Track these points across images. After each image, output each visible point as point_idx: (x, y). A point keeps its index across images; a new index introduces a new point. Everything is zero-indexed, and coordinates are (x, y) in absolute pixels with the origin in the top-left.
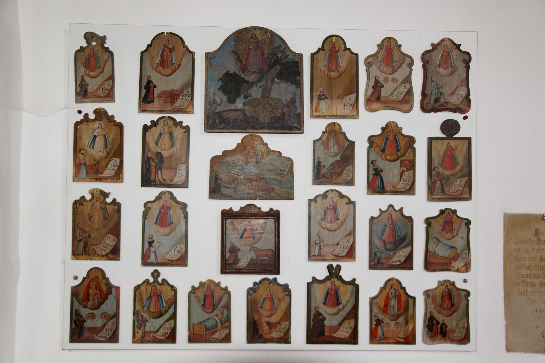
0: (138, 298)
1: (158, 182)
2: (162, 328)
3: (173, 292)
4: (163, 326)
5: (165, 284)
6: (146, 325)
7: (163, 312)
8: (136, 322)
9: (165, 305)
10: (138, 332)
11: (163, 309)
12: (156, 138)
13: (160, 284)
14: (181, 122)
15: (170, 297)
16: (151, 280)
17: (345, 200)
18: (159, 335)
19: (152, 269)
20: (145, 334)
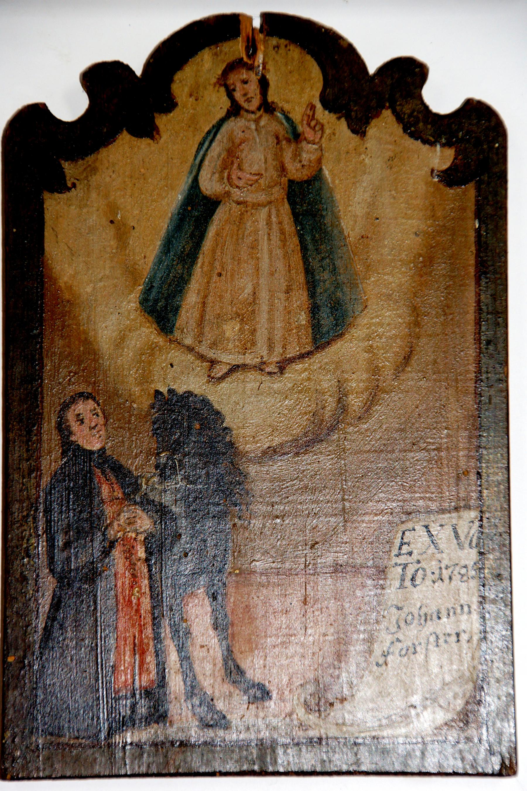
1: (184, 720)
12: (147, 249)
14: (408, 73)
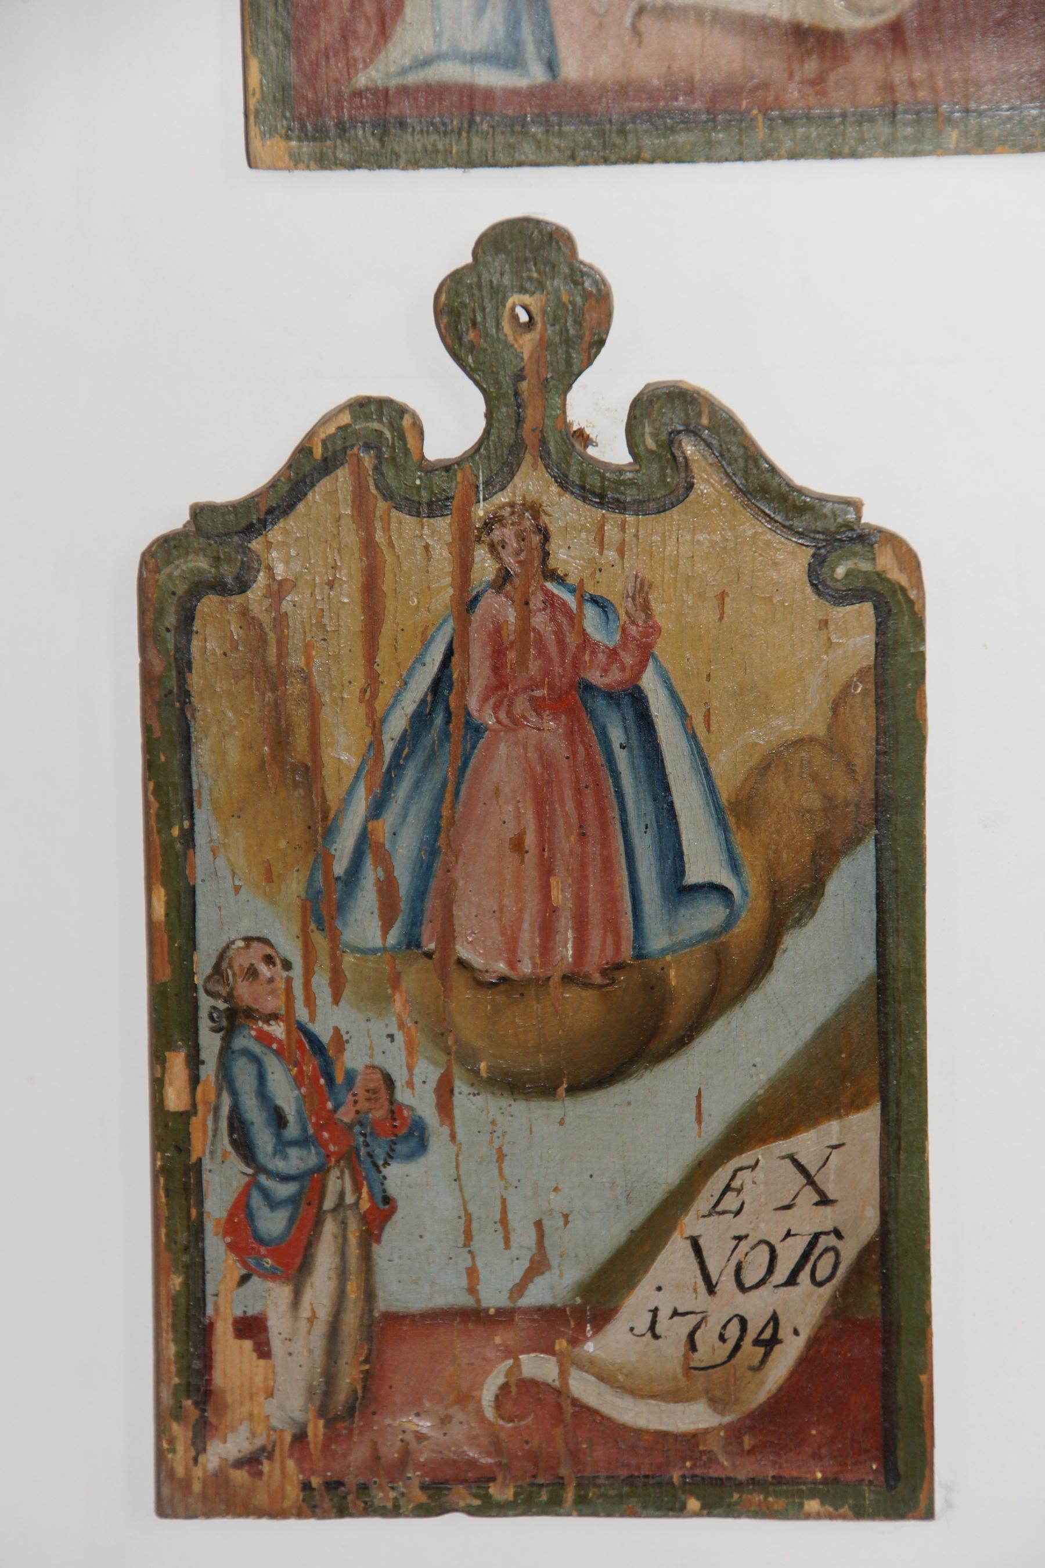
0: (222, 751)
2: (673, 1260)
3: (856, 631)
4: (692, 1223)
5: (708, 483)
6: (384, 1208)
7: (683, 980)
8: (211, 1144)
9: (704, 862)
10: (251, 1328)
11: (673, 934)
13: (600, 490)
15: (804, 715)
16: (451, 419)
17: (668, 505)
18: (627, 1373)
19: (437, 215)
20: (379, 1341)
